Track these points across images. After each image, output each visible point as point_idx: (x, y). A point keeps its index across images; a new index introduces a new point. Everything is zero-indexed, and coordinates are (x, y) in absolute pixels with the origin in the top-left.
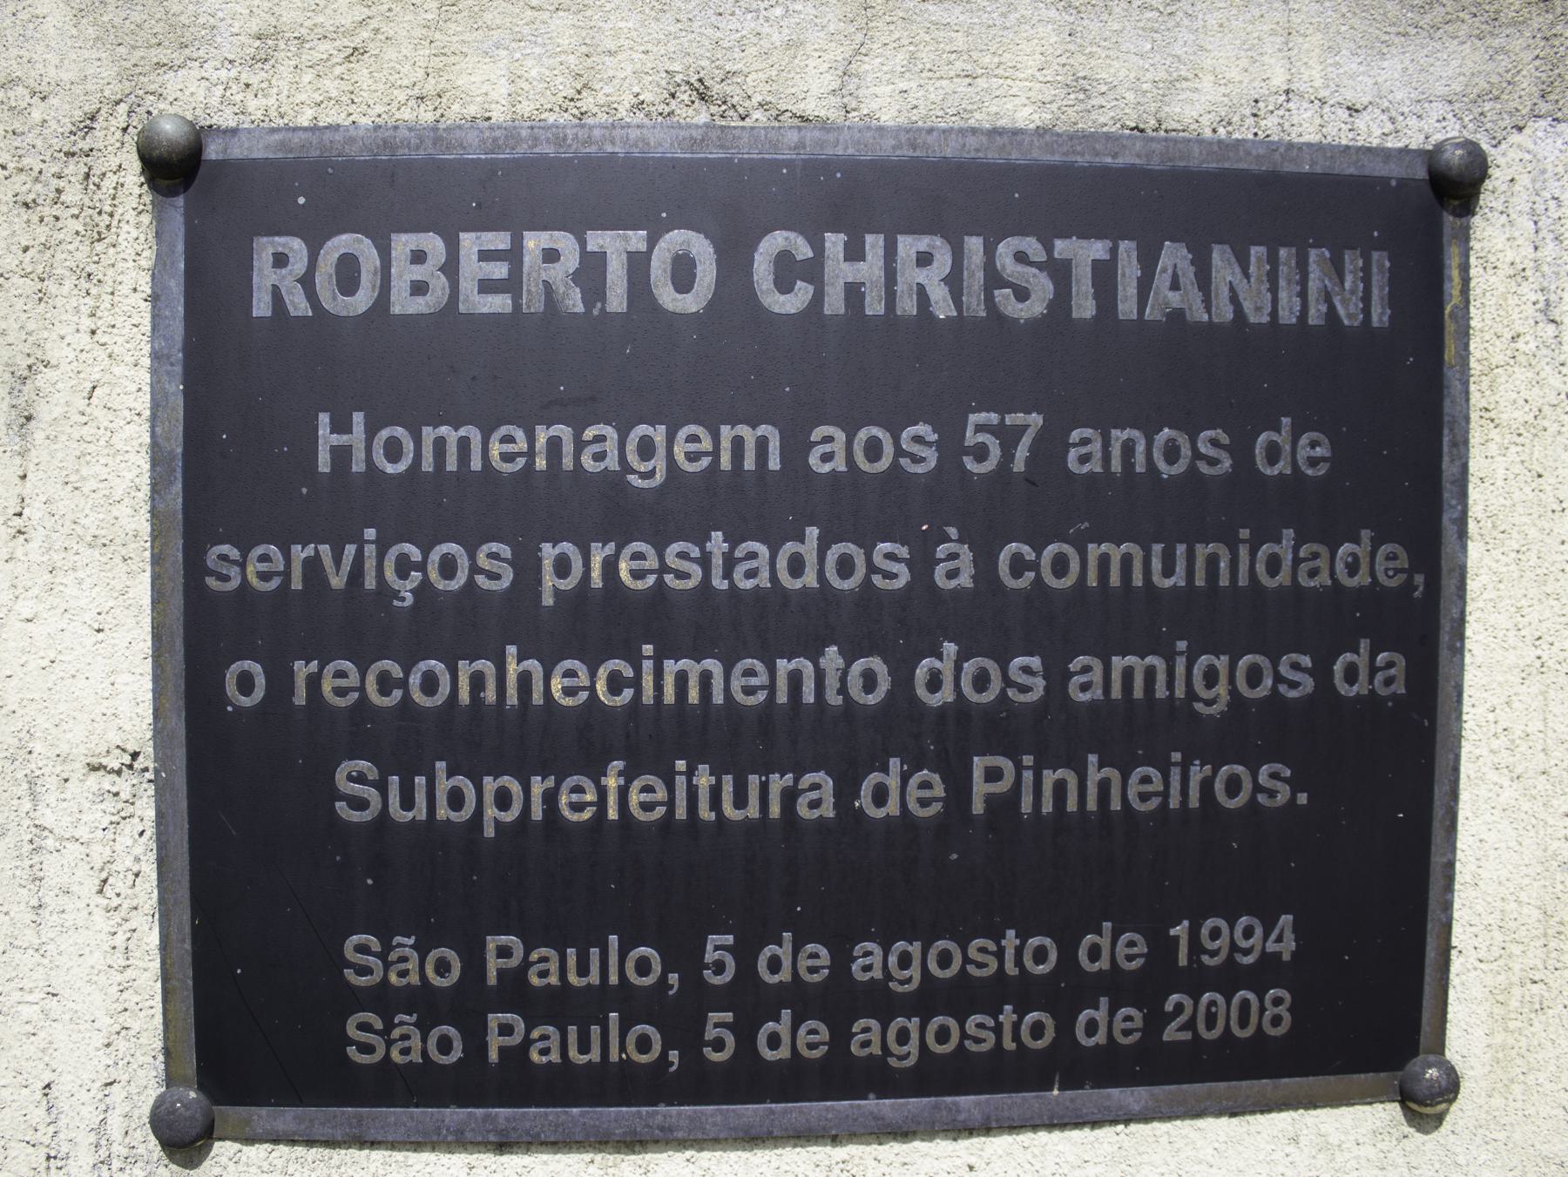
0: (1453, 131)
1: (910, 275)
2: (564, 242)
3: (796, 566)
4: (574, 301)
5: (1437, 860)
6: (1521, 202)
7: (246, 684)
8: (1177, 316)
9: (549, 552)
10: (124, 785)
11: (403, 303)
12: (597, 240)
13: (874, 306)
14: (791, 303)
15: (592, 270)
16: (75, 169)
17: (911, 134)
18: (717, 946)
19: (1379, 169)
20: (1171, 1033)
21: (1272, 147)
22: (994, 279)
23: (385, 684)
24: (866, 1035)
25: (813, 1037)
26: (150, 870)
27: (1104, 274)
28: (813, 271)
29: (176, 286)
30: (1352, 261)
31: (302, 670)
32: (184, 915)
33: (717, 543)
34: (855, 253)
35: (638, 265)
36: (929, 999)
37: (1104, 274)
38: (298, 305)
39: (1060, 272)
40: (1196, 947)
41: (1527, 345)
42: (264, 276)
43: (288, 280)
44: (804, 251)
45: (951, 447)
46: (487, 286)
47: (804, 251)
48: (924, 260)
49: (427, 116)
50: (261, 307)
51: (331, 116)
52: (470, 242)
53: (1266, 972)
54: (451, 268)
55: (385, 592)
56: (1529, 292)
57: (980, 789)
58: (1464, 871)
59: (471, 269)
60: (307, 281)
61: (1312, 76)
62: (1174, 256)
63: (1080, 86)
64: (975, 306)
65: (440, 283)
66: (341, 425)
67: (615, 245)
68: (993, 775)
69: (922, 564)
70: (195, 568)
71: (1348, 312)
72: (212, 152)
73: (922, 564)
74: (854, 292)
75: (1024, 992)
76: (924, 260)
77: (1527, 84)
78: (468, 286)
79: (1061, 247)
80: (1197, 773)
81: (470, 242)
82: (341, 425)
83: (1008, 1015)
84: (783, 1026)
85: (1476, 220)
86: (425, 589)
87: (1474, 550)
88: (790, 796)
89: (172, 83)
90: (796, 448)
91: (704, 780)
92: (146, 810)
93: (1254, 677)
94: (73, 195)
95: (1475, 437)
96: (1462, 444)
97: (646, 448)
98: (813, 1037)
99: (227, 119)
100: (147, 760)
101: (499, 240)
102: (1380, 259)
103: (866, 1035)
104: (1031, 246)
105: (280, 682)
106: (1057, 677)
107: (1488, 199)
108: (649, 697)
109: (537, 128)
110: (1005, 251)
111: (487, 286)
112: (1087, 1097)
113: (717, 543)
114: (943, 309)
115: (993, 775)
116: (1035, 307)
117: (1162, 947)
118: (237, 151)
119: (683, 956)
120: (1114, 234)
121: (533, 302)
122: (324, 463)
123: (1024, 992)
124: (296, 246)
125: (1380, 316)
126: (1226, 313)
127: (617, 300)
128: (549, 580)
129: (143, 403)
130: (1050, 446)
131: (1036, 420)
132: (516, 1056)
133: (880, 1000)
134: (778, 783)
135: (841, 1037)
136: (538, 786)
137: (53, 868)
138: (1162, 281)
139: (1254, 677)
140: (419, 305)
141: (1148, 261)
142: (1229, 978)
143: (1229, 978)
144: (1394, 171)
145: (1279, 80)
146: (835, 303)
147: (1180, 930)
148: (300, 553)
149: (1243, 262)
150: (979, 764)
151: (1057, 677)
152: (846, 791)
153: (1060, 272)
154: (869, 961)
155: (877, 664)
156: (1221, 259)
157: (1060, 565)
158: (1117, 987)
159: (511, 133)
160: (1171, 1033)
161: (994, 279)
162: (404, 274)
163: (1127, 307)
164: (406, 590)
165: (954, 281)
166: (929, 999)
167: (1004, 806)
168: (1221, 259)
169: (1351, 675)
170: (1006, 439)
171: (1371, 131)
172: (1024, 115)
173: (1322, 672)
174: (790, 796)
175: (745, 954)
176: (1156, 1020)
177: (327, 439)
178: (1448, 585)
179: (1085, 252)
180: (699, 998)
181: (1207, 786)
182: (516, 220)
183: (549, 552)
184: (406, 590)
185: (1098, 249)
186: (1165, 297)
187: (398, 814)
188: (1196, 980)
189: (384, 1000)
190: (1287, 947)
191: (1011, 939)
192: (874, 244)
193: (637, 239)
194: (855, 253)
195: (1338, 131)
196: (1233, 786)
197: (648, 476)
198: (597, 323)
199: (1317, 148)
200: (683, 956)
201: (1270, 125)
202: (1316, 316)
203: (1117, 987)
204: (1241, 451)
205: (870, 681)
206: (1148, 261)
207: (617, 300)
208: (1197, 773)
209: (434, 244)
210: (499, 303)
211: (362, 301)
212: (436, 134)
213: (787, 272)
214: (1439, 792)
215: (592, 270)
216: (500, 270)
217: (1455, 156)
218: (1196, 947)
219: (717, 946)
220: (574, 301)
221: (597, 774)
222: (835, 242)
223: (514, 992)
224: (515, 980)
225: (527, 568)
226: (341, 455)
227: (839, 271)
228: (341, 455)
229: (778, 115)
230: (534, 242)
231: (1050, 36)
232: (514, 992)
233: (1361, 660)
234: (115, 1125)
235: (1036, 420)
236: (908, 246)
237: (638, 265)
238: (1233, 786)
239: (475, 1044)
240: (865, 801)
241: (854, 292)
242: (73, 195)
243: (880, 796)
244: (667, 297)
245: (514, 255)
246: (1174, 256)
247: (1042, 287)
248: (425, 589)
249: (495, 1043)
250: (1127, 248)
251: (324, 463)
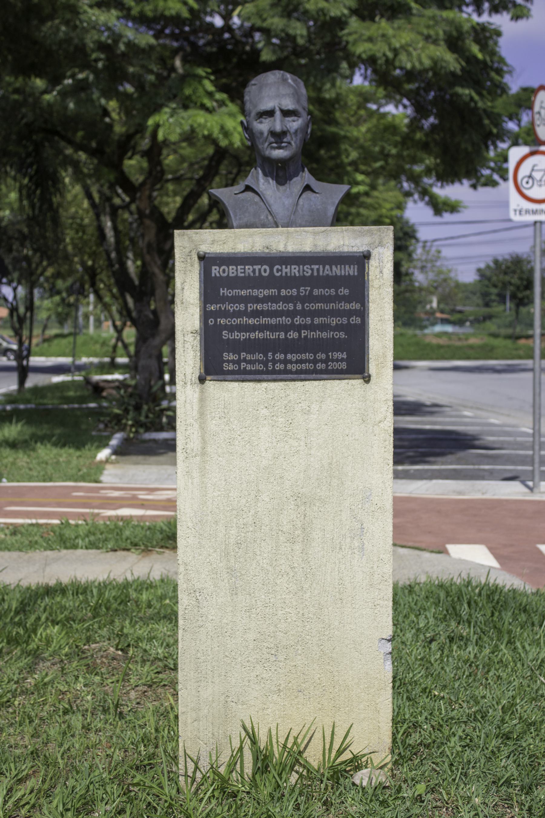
0: (367, 249)
1: (293, 271)
2: (251, 267)
3: (279, 307)
4: (252, 274)
5: (366, 346)
6: (377, 258)
7: (211, 322)
8: (328, 275)
9: (249, 305)
10: (195, 335)
11: (231, 275)
12: (255, 267)
13: (289, 275)
14: (278, 274)
15: (254, 271)
16: (189, 257)
17: (293, 253)
18: (270, 354)
19: (356, 254)
20: (330, 368)
21: (341, 252)
22: (304, 271)
23: (229, 321)
24: (289, 366)
25: (282, 367)
26: (199, 346)
27: (318, 270)
28: (281, 270)
29: (202, 272)
30: (352, 266)
31: (219, 320)
32: (203, 351)
33: (270, 304)
34: (286, 268)
35: (260, 270)
36: (297, 362)
37: (318, 270)
38: (218, 275)
39: (312, 270)
40: (332, 356)
41: (378, 277)
42: (213, 271)
43: (216, 272)
44: (280, 268)
45: (298, 292)
46: (241, 273)
47: (280, 268)
48: (295, 269)
49: (233, 251)
50: (213, 275)
51: (221, 251)
52: (239, 267)
53: (342, 360)
54: (237, 270)
55: (229, 310)
56: (378, 270)
57: (303, 335)
58: (371, 347)
59: (239, 271)
60: (219, 272)
61: (347, 243)
62: (327, 267)
63: (315, 246)
64: (301, 274)
65: (235, 272)
66: (223, 290)
67: (257, 267)
68: (304, 333)
69: (295, 306)
70: (205, 307)
71: (352, 273)
72: (207, 256)
73: (295, 306)
74: (286, 273)
75: (309, 361)
76: (295, 269)
77: (377, 242)
78: (239, 272)
79: (313, 266)
80: (332, 333)
81: (239, 267)
82: (223, 290)
83: (307, 364)
84: (278, 365)
85: (370, 261)
86: (234, 310)
87: (370, 304)
88: (279, 335)
89: (201, 247)
90: (279, 292)
91: (268, 333)
92: (198, 338)
93: (339, 321)
94: (189, 261)
95: (370, 289)
96: (368, 290)
97: (261, 292)
98: (282, 367)
99: (208, 251)
100: (199, 332)
101: (243, 267)
102: (356, 266)
103: (289, 366)
104: (309, 266)
105: (216, 321)
106: (312, 321)
107: (372, 257)
108: (295, 28)
109: (247, 253)
110: (305, 267)
111: (241, 273)
112: (319, 376)
113: (270, 304)
114: (297, 275)
115: (304, 333)
116: (309, 274)
117: (328, 356)
118: (210, 256)
119: (266, 355)
120: (319, 264)
121: (247, 275)
122: (221, 294)
123: (309, 361)
124: (217, 268)
125: (356, 274)
126: (334, 274)
127: (257, 274)
128: (249, 309)
129: (198, 287)
130: (311, 291)
131: (309, 288)
132: (245, 368)
133: (291, 362)
134: (277, 334)
135: (286, 367)
136: (248, 334)
137: (186, 346)
138: (326, 270)
139: (339, 321)
140: (233, 275)
141: (324, 268)
142: (337, 361)
143: (337, 361)
144: (358, 255)
145: (342, 243)
146: (284, 274)
147: (330, 354)
148: (218, 306)
149: (337, 267)
150: (303, 331)
151: (312, 321)
152: (286, 335)
153: (312, 270)
154: (289, 356)
155: (289, 319)
156: (334, 268)
157: (313, 306)
158: (322, 361)
159: (244, 253)
160: (330, 368)
161: (304, 271)
162: (231, 271)
163: (321, 274)
164: (232, 310)
165: (299, 271)
166: (297, 362)
167: (306, 337)
168: (334, 268)
169: (353, 321)
170: (306, 290)
171: (355, 249)
172: (308, 250)
173: (348, 320)
174: (279, 335)
175: (273, 355)
176: (327, 366)
177: (222, 291)
178: (366, 309)
179: (315, 267)
180: (268, 361)
181: (333, 335)
182: (245, 265)
183: (249, 305)
184: (232, 310)
185: (317, 267)
186: (326, 272)
187: (230, 338)
188: (333, 361)
189: (228, 361)
190: (345, 357)
191: (307, 354)
192: (289, 267)
193: (260, 267)
194: (286, 268)
195: (351, 250)
196: (337, 335)
197: (261, 296)
198: (255, 277)
199: (348, 252)
200: (266, 355)
201: (341, 249)
202: (347, 274)
203: (322, 361)
204: (336, 292)
205: (288, 321)
206: (324, 268)
207: (257, 274)
208: (332, 333)
209: (234, 267)
210: (243, 275)
211: (226, 274)
212: (234, 253)
213: (278, 270)
214: (366, 336)
215: (254, 271)
216: (243, 271)
217: (365, 253)
218: (332, 356)
219: (270, 354)
220: (252, 274)
221: (255, 332)
222: (284, 267)
223: (245, 360)
224: (244, 359)
225: (246, 307)
226: (223, 293)
227: (284, 270)
228: (223, 293)
229: (173, 670)
230: (247, 267)
231: (311, 239)
232: (245, 360)
233: (354, 319)
234: (193, 379)
235: (309, 288)
236: (293, 267)
237: (260, 270)
238: (337, 335)
239: (240, 367)
240: (288, 336)
241: (286, 273)
242: (189, 261)
243: (290, 335)
244: (263, 274)
245: (244, 269)
246: (327, 267)
247: (310, 272)
248: (234, 310)
249: (242, 367)
250: (321, 266)
251: (221, 294)
